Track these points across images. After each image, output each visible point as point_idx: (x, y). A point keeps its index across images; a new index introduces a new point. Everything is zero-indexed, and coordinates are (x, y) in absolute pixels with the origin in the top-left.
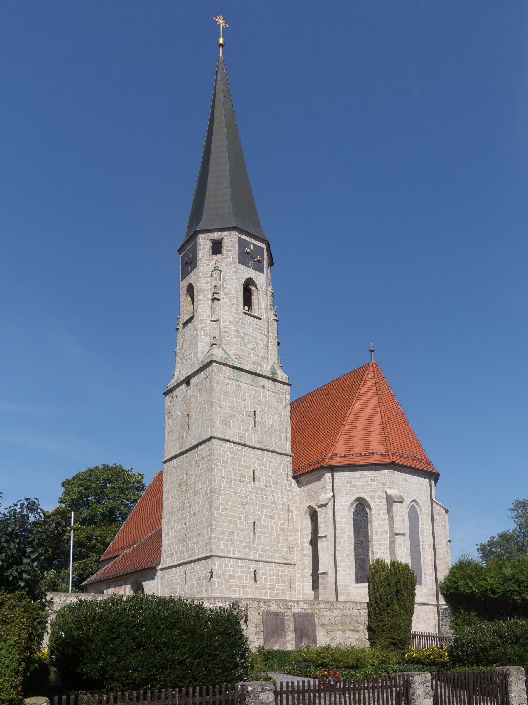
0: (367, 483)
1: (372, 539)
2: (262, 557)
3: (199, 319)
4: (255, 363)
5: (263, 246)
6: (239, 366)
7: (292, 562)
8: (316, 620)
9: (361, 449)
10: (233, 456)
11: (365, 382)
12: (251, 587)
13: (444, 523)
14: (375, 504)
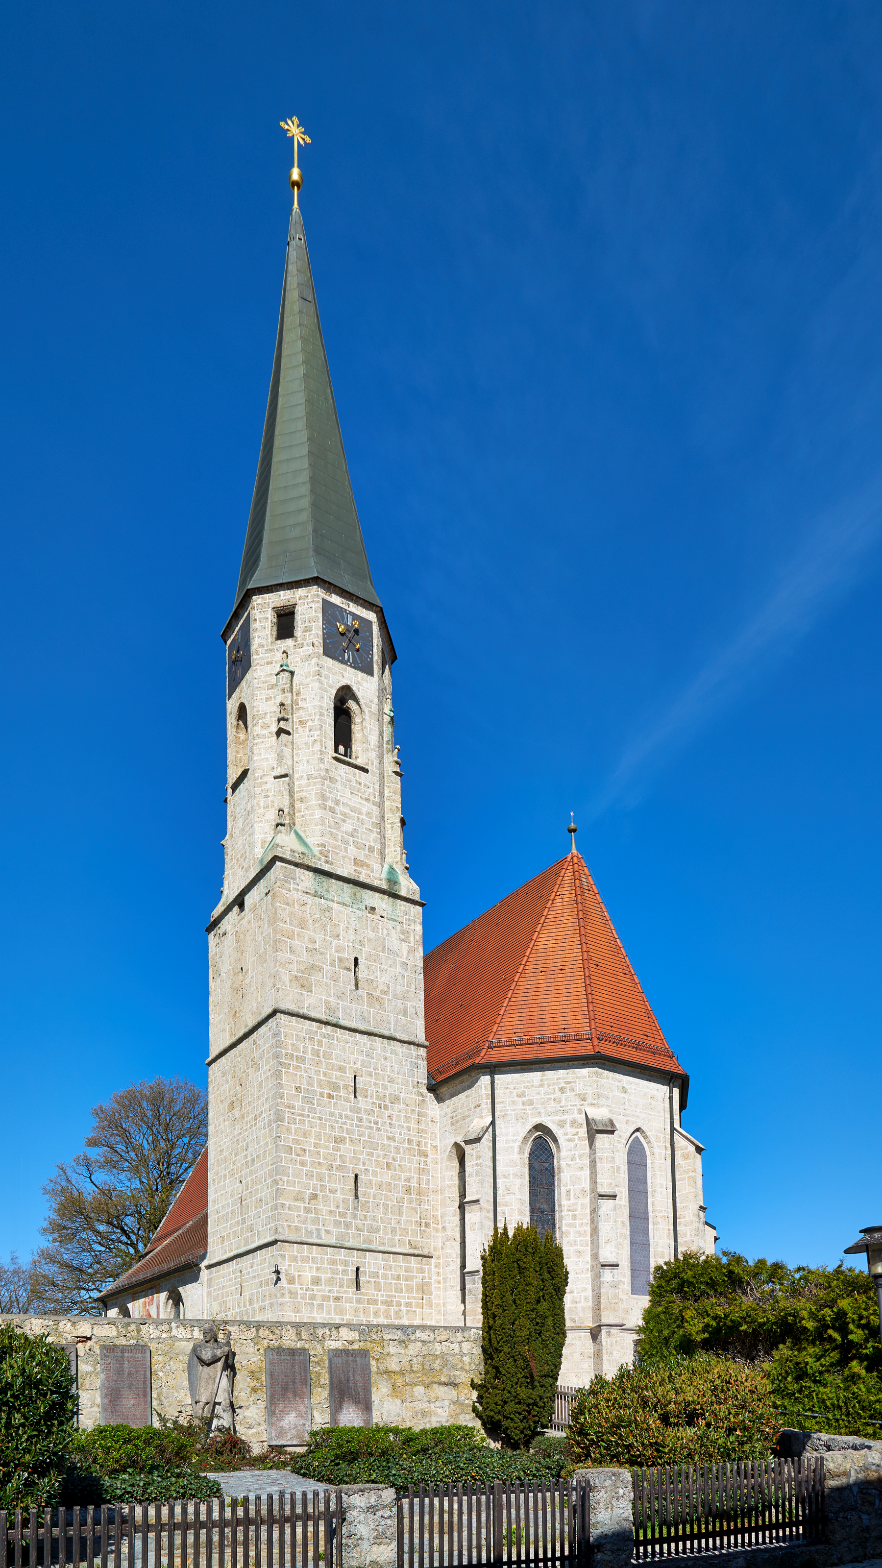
0: (552, 1096)
1: (560, 1205)
2: (370, 1242)
3: (256, 775)
4: (356, 862)
5: (371, 616)
6: (326, 868)
7: (426, 1253)
8: (373, 1362)
9: (544, 1028)
10: (316, 1047)
11: (558, 894)
12: (350, 1300)
13: (693, 1174)
14: (567, 1137)
